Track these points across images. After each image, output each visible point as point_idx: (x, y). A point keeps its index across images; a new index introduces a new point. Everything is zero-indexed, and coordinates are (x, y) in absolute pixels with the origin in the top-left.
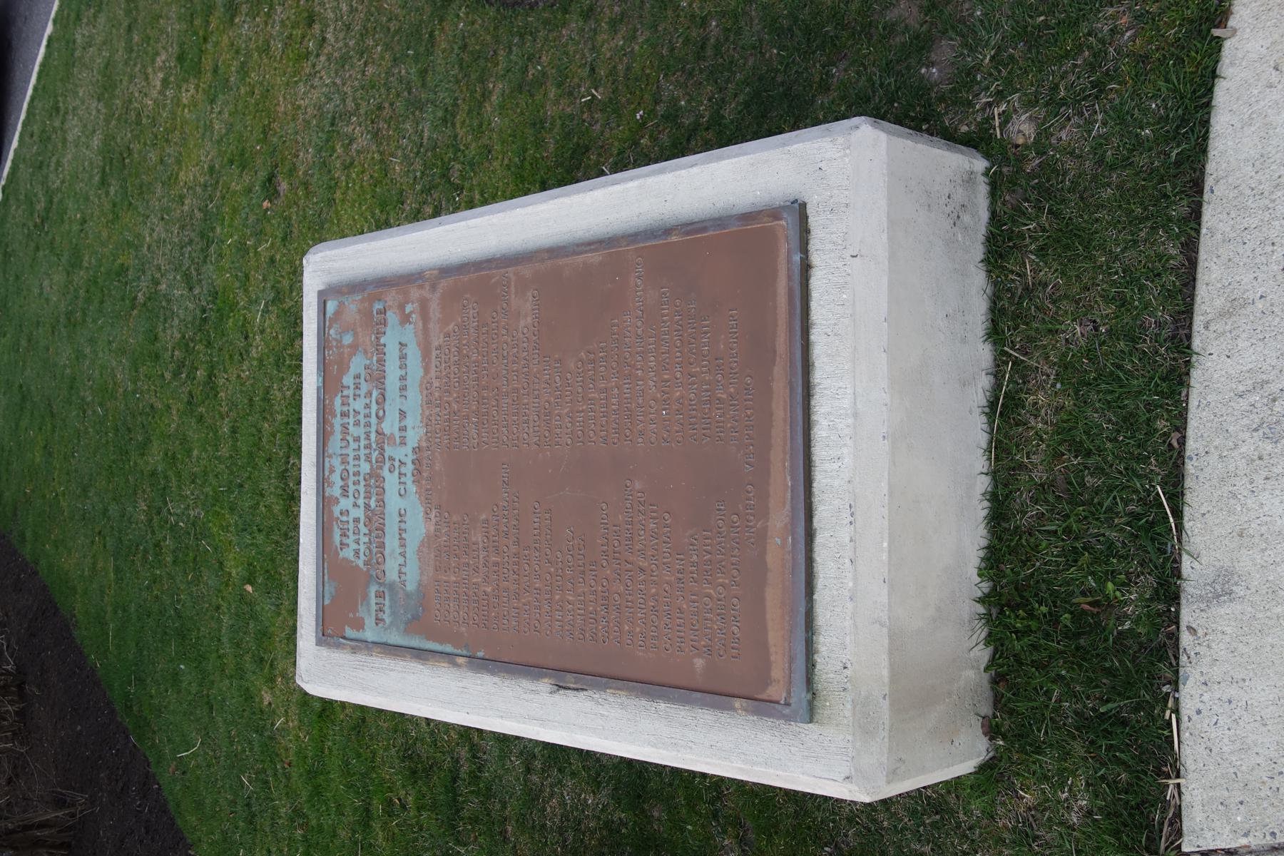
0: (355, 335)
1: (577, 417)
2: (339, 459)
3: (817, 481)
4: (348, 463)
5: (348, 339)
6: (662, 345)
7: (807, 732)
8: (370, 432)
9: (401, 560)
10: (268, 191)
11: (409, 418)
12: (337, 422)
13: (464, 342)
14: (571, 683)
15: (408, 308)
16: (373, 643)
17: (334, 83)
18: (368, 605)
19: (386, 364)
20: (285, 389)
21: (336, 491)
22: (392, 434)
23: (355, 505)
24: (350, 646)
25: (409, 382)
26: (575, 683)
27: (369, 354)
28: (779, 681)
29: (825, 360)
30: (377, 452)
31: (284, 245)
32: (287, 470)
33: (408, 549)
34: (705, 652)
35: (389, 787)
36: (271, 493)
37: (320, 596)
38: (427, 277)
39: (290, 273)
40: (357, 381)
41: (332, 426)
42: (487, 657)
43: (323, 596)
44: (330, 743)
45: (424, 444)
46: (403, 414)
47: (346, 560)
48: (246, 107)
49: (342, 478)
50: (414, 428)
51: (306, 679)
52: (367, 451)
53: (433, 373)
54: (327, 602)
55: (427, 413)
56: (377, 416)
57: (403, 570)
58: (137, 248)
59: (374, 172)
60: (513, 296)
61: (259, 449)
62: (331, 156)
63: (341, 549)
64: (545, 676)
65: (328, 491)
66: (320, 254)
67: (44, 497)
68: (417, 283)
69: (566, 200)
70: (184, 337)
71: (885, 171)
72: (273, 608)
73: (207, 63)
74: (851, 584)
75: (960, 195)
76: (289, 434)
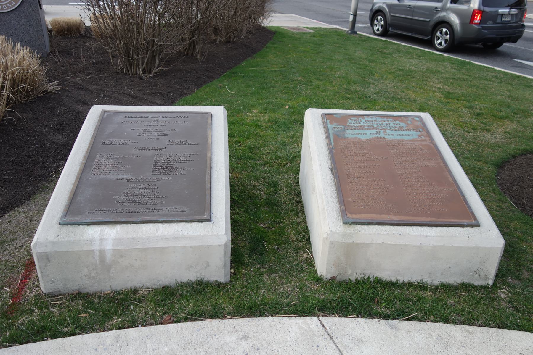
0: (411, 124)
5: (409, 122)
11: (393, 136)
17: (456, 135)
21: (366, 118)
22: (386, 132)
25: (402, 136)
37: (336, 114)
46: (393, 135)
47: (348, 121)
48: (439, 111)
51: (311, 110)
53: (406, 142)
58: (382, 79)
65: (366, 117)
67: (290, 50)
70: (358, 91)
73: (450, 100)
74: (382, 233)
75: (483, 274)
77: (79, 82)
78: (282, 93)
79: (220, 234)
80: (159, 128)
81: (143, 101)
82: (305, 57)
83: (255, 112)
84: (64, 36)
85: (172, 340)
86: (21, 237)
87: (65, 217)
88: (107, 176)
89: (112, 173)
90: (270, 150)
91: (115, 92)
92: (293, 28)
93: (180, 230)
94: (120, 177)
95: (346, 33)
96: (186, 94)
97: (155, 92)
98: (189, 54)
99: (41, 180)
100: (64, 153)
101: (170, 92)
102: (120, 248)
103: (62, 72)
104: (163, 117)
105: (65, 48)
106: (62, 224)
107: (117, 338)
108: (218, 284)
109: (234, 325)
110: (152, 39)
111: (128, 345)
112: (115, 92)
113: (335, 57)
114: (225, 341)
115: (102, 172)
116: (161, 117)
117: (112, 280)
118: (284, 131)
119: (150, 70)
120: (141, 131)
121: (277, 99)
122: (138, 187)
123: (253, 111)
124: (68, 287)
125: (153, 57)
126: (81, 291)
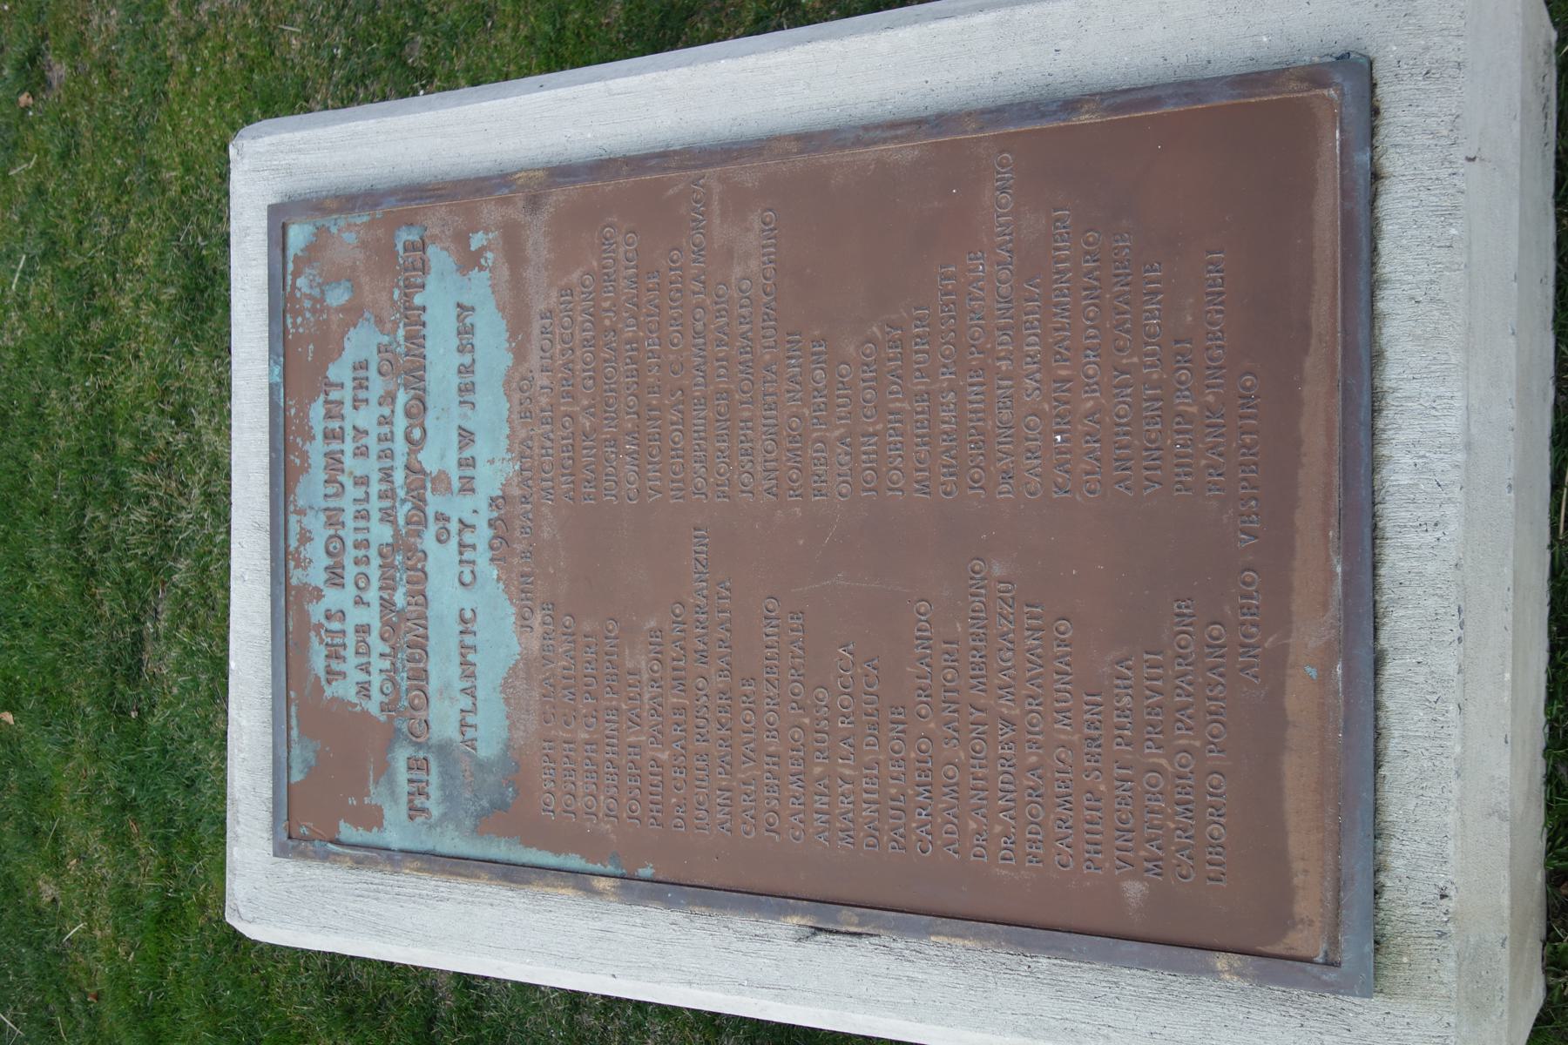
0: (356, 288)
1: (864, 444)
2: (322, 517)
3: (1388, 563)
4: (343, 524)
5: (338, 297)
6: (1056, 315)
7: (1360, 1010)
8: (392, 468)
9: (466, 702)
10: (28, 78)
12: (317, 450)
13: (606, 305)
14: (852, 924)
15: (477, 241)
16: (402, 851)
18: (392, 782)
19: (428, 344)
20: (74, 398)
21: (316, 575)
23: (359, 601)
24: (352, 857)
25: (479, 377)
26: (860, 924)
27: (388, 326)
28: (1311, 923)
29: (1409, 346)
30: (408, 506)
31: (65, 166)
32: (80, 528)
33: (479, 683)
34: (1148, 870)
35: (301, 1035)
36: (49, 566)
37: (281, 767)
38: (519, 182)
39: (76, 211)
40: (362, 373)
41: (304, 456)
42: (660, 878)
43: (289, 767)
44: (177, 964)
45: (516, 492)
46: (466, 437)
49: (328, 553)
50: (492, 462)
52: (387, 503)
54: (297, 777)
55: (523, 434)
56: (408, 439)
57: (470, 719)
59: (247, 47)
60: (717, 221)
61: (23, 495)
62: (156, 22)
63: (329, 682)
64: (794, 911)
65: (297, 577)
66: (267, 140)
68: (497, 195)
69: (834, 46)
71: (1519, 9)
72: (56, 749)
74: (1458, 749)
76: (84, 472)
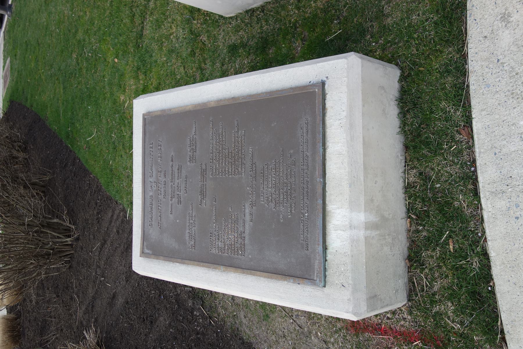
67: (35, 79)
77: (83, 309)
78: (95, 72)
79: (346, 66)
80: (169, 178)
81: (108, 232)
82: (44, 58)
83: (123, 98)
84: (20, 335)
85: (505, 118)
86: (310, 344)
87: (314, 280)
88: (247, 235)
89: (241, 229)
90: (181, 66)
91: (97, 265)
92: (5, 82)
93: (338, 122)
94: (248, 218)
95: (10, 18)
96: (98, 186)
97: (97, 219)
98: (44, 190)
99: (222, 334)
100: (183, 312)
101: (96, 204)
102: (363, 202)
103: (69, 331)
104: (151, 176)
105: (37, 332)
106: (324, 283)
107: (494, 194)
108: (403, 78)
109: (481, 39)
110: (26, 226)
111: (511, 177)
112: (97, 265)
113: (44, 22)
114: (511, 44)
115: (239, 243)
116: (151, 180)
117: (396, 217)
118: (151, 56)
119: (66, 230)
120: (173, 201)
121: (104, 76)
122: (265, 191)
123: (122, 100)
124: (401, 272)
125: (49, 226)
126: (406, 256)
